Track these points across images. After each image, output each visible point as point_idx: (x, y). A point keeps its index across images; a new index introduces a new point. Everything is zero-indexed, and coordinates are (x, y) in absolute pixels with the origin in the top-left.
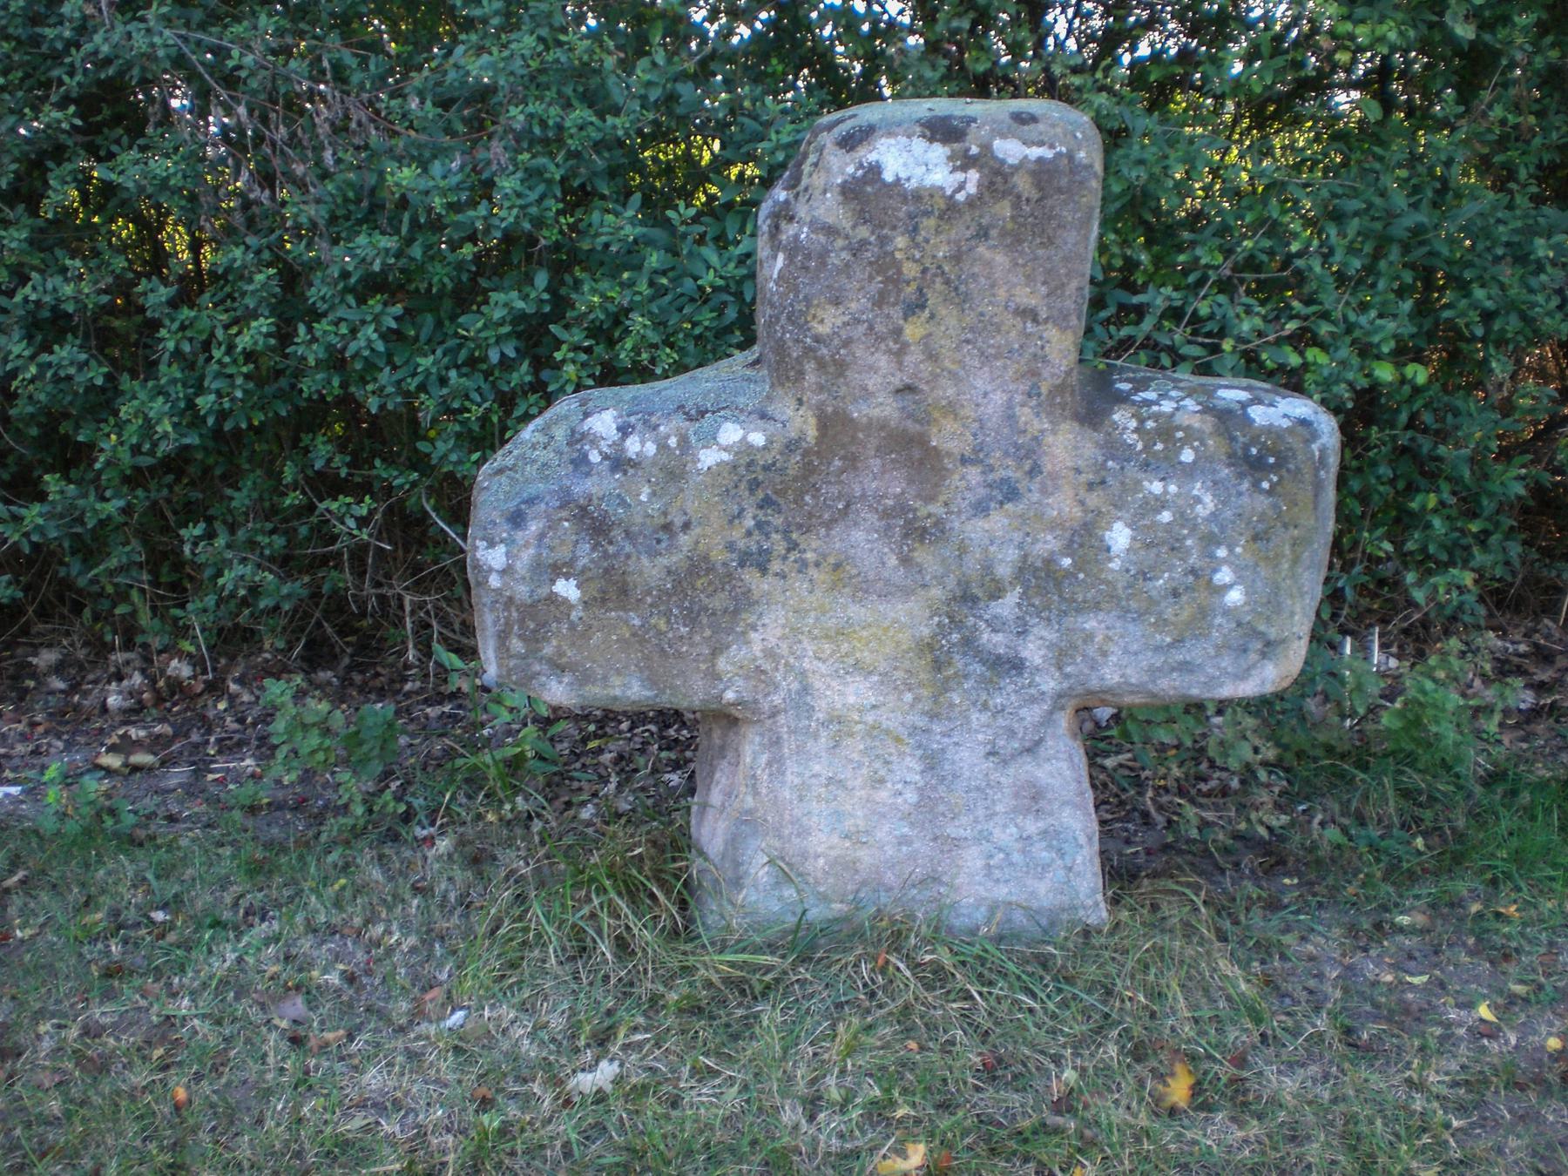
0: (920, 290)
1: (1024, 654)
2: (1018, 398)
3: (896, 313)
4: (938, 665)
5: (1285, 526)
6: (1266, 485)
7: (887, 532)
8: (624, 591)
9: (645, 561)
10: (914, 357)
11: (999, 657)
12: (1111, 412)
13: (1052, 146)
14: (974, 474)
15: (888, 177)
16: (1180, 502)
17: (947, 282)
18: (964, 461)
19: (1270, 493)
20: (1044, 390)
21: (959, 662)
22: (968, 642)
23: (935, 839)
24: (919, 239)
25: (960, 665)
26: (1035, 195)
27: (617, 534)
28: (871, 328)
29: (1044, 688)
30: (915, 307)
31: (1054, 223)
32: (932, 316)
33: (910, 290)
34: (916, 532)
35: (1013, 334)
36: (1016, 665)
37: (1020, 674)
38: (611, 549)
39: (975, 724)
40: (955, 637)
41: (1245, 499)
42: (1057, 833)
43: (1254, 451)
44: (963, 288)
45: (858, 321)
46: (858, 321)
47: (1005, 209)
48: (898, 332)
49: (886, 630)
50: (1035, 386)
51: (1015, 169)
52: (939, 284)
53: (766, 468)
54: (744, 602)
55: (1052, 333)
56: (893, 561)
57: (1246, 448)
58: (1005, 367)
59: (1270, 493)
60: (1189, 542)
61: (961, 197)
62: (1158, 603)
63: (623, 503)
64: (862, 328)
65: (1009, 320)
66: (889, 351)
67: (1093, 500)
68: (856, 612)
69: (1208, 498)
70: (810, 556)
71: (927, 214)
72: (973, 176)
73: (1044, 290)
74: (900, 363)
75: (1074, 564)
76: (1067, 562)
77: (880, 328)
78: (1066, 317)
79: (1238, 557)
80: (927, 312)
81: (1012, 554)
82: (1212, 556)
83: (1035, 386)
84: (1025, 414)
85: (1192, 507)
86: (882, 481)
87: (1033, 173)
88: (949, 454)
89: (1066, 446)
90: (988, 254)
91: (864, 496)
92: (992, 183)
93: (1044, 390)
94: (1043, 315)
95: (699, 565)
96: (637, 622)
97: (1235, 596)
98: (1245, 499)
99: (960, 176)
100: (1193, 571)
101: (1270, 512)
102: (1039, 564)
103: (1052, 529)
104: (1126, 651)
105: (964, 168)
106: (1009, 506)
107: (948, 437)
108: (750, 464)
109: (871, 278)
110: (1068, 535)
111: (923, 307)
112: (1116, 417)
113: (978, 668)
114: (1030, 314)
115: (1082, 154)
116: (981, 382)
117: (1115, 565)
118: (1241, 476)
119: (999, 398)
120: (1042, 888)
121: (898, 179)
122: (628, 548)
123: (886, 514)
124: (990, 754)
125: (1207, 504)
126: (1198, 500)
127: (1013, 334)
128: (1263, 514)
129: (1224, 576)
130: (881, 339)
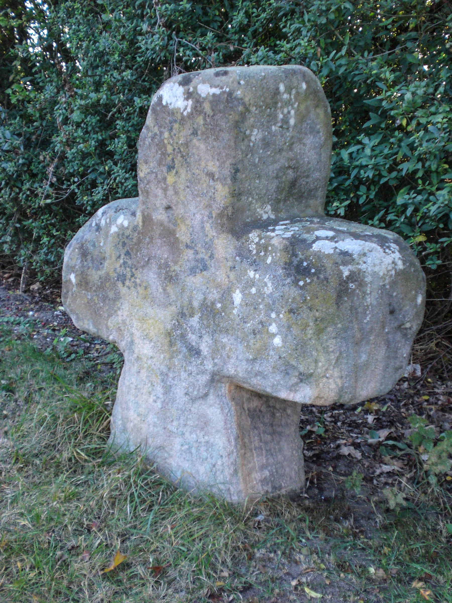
0: (173, 159)
1: (201, 348)
2: (206, 218)
3: (165, 169)
4: (171, 344)
5: (311, 309)
6: (301, 283)
7: (159, 274)
8: (87, 283)
9: (94, 271)
10: (170, 192)
11: (193, 346)
12: (250, 232)
13: (222, 88)
14: (190, 254)
15: (164, 103)
16: (260, 284)
17: (182, 156)
18: (187, 246)
19: (301, 288)
20: (214, 216)
21: (179, 344)
22: (183, 336)
23: (165, 428)
24: (172, 134)
25: (179, 346)
26: (212, 114)
27: (89, 257)
28: (156, 176)
29: (206, 367)
30: (171, 168)
31: (218, 128)
32: (177, 173)
33: (170, 159)
34: (170, 278)
35: (205, 185)
36: (198, 353)
37: (198, 358)
38: (85, 263)
39: (182, 378)
40: (179, 332)
41: (287, 288)
42: (212, 445)
43: (305, 264)
44: (188, 160)
45: (152, 172)
46: (152, 172)
47: (200, 120)
48: (165, 179)
49: (156, 321)
50: (211, 213)
51: (205, 99)
52: (179, 158)
53: (127, 237)
54: (117, 297)
55: (219, 186)
56: (161, 290)
57: (301, 262)
58: (200, 201)
59: (301, 288)
60: (261, 306)
61: (185, 113)
62: (247, 336)
63: (94, 246)
64: (154, 175)
65: (204, 178)
66: (162, 188)
67: (232, 275)
68: (150, 311)
69: (269, 285)
70: (138, 281)
71: (175, 121)
72: (190, 102)
73: (218, 163)
74: (166, 194)
75: (222, 308)
76: (219, 305)
77: (159, 176)
78: (225, 179)
79: (280, 319)
80: (174, 172)
81: (200, 297)
82: (269, 316)
83: (211, 213)
84: (208, 226)
85: (263, 287)
86: (161, 251)
87: (211, 102)
88: (182, 242)
89: (224, 246)
90: (197, 144)
91: (155, 256)
92: (196, 107)
93: (214, 216)
94: (216, 177)
95: (107, 278)
96: (89, 297)
97: (277, 341)
98: (287, 288)
99: (186, 102)
100: (261, 323)
101: (298, 298)
102: (209, 304)
103: (217, 288)
104: (237, 358)
105: (187, 99)
106: (204, 273)
107: (183, 235)
108: (123, 234)
109: (157, 152)
110: (222, 292)
111: (173, 168)
112: (250, 235)
113: (184, 350)
114: (211, 175)
115: (239, 92)
116: (192, 208)
117: (235, 311)
118: (289, 275)
119: (198, 217)
120: (202, 470)
121: (167, 104)
122: (90, 265)
123: (160, 268)
124: (186, 394)
125: (269, 289)
126: (266, 285)
127: (205, 185)
128: (294, 298)
129: (273, 328)
130: (159, 182)
